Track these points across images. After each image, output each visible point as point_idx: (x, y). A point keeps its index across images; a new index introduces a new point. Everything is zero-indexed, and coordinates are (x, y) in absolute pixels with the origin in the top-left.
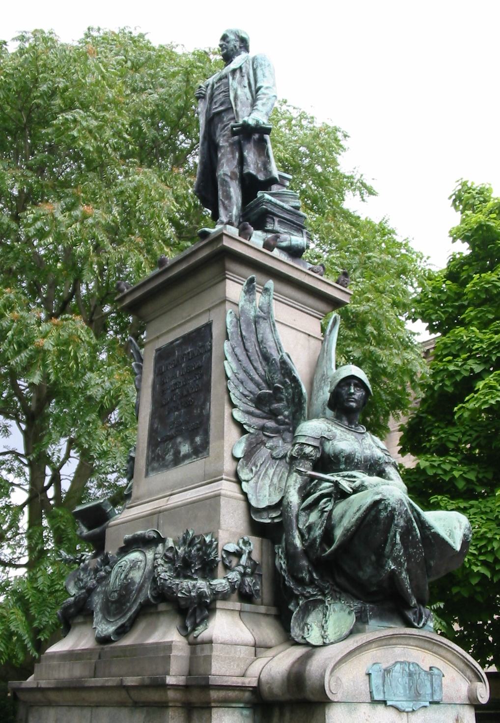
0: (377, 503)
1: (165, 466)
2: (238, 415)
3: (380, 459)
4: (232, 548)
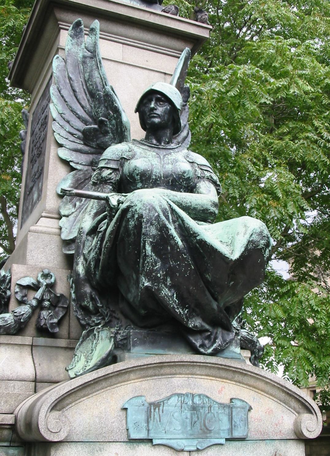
2: (64, 154)
3: (184, 172)
4: (25, 282)
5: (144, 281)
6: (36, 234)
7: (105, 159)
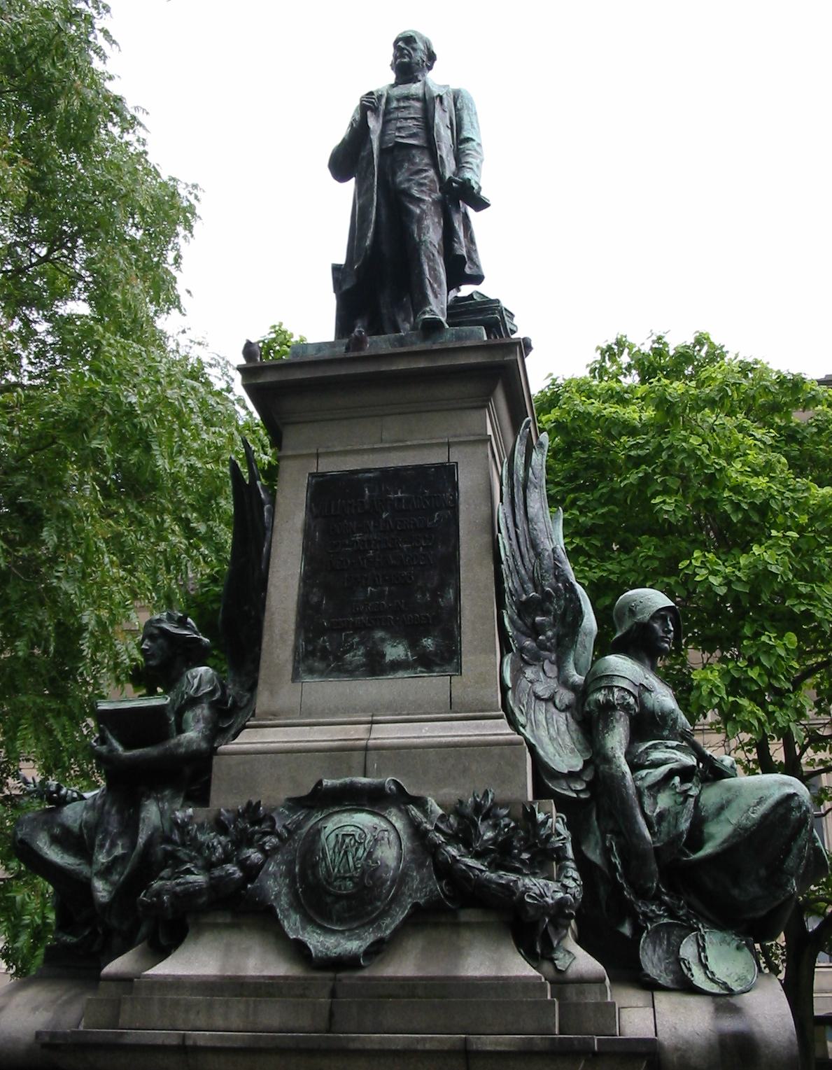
0: (795, 794)
1: (341, 669)
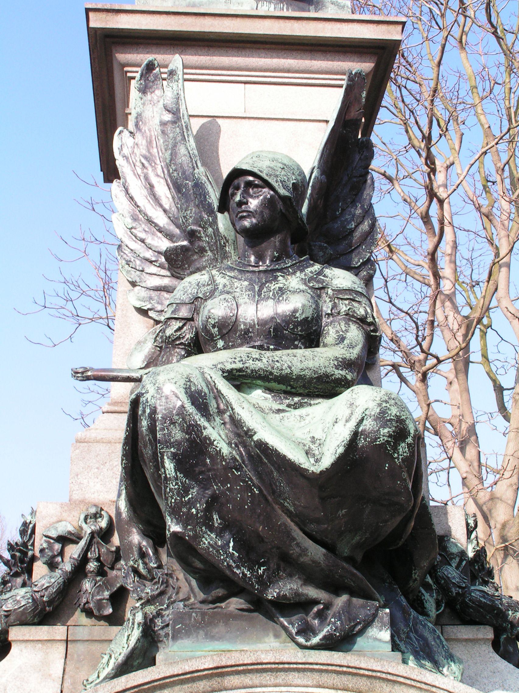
5: (170, 523)
6: (86, 444)
7: (173, 303)
